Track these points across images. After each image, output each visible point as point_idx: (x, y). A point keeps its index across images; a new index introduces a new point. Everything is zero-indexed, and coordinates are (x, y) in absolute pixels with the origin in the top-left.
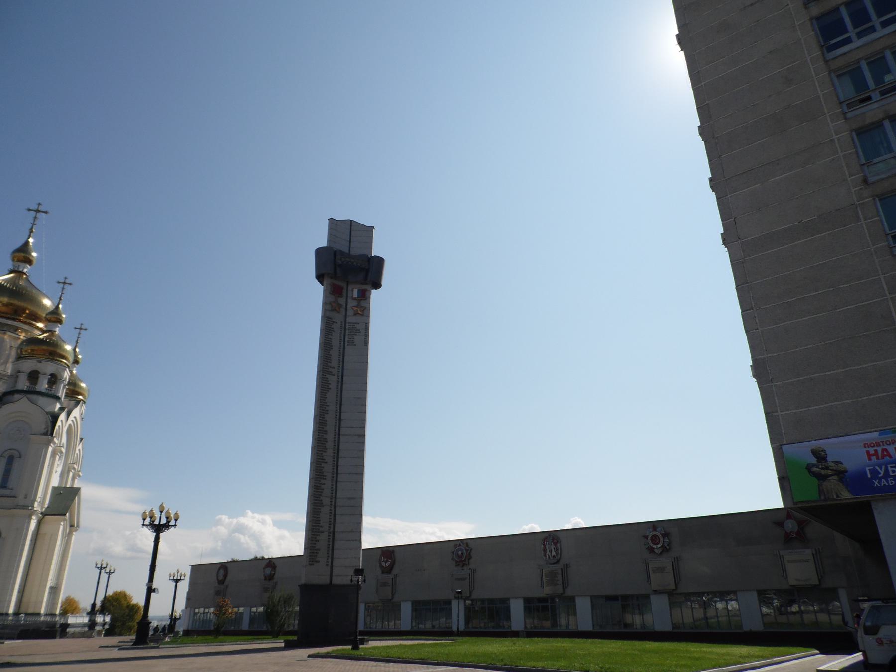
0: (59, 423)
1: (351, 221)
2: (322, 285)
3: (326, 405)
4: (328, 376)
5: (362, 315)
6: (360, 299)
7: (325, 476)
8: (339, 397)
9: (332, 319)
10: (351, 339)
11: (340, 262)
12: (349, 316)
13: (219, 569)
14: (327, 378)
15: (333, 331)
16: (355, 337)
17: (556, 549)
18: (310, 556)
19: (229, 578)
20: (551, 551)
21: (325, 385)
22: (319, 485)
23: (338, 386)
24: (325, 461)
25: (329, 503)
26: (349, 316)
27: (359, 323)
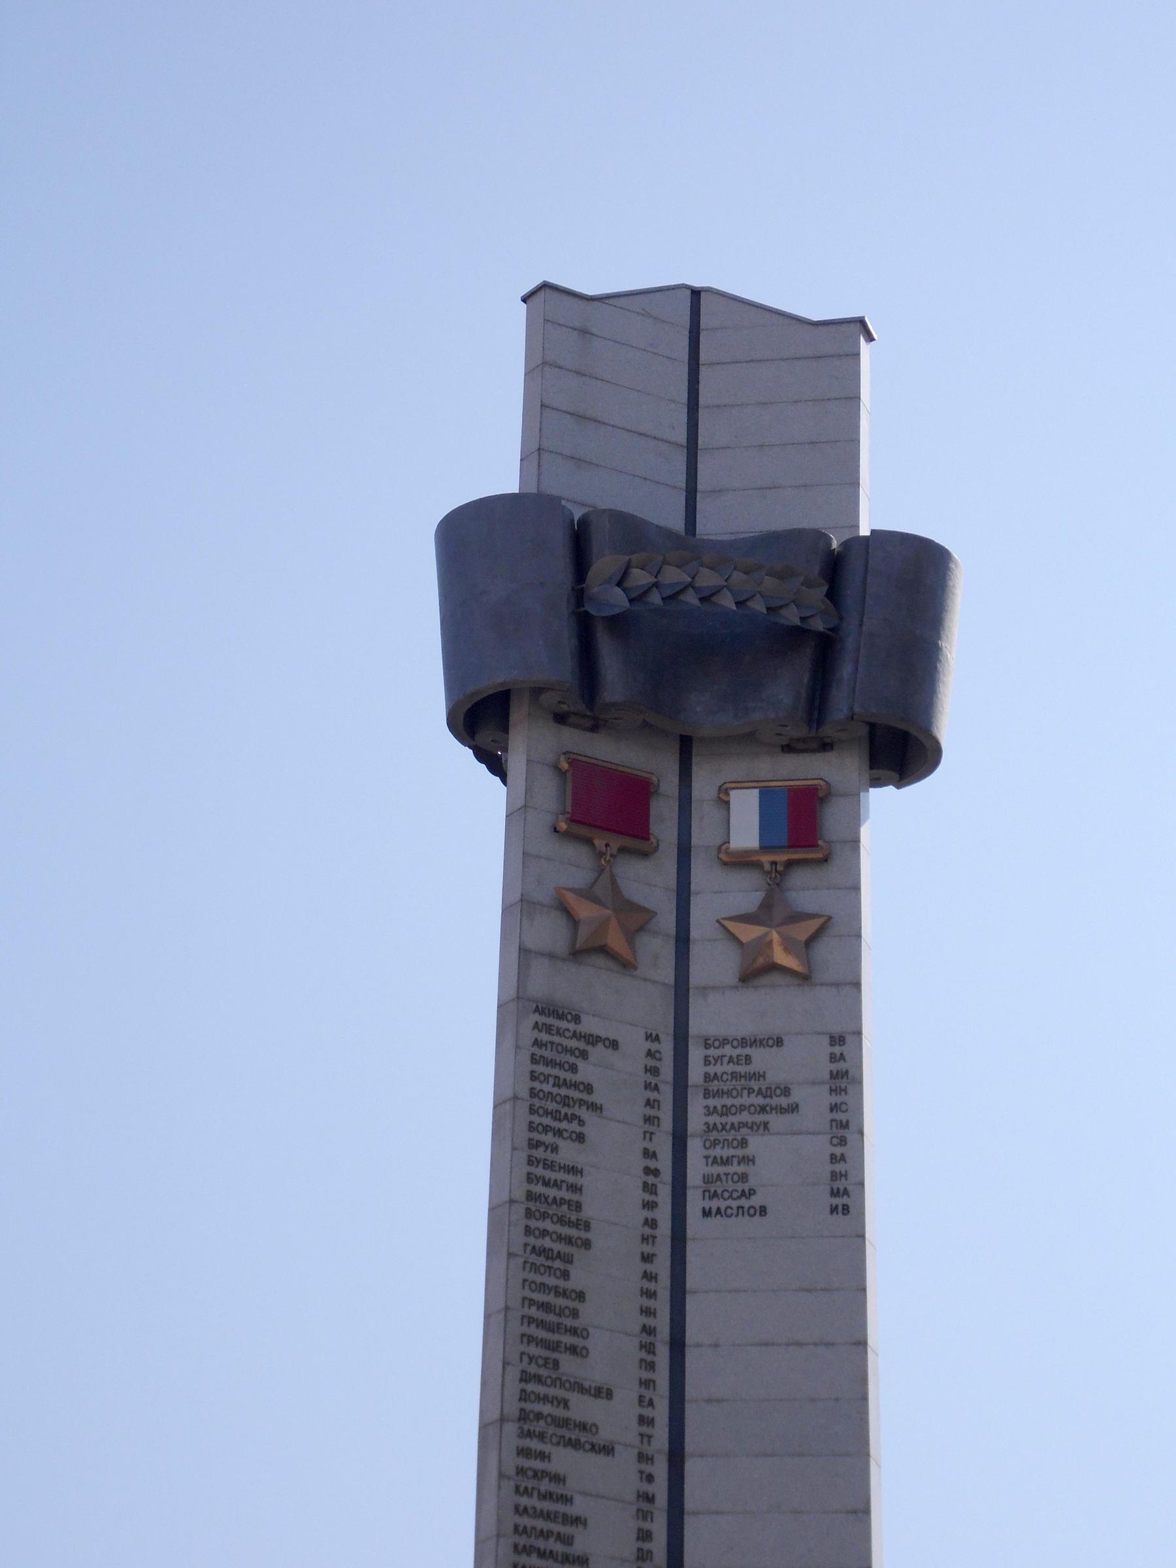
1: (696, 293)
2: (497, 767)
4: (563, 1460)
5: (805, 979)
6: (782, 858)
9: (577, 1019)
10: (726, 1162)
11: (618, 599)
12: (705, 990)
14: (558, 1479)
15: (595, 1108)
16: (757, 1144)
21: (544, 1534)
23: (645, 1536)
26: (705, 990)
27: (779, 1042)
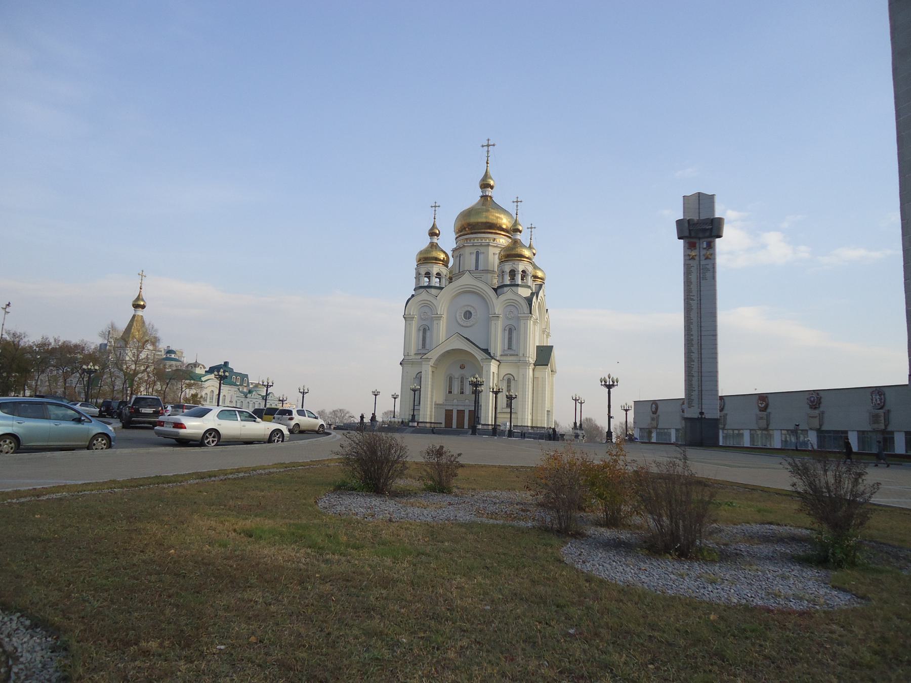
0: (533, 304)
4: (691, 301)
8: (699, 313)
13: (652, 404)
17: (881, 399)
19: (658, 411)
20: (876, 400)
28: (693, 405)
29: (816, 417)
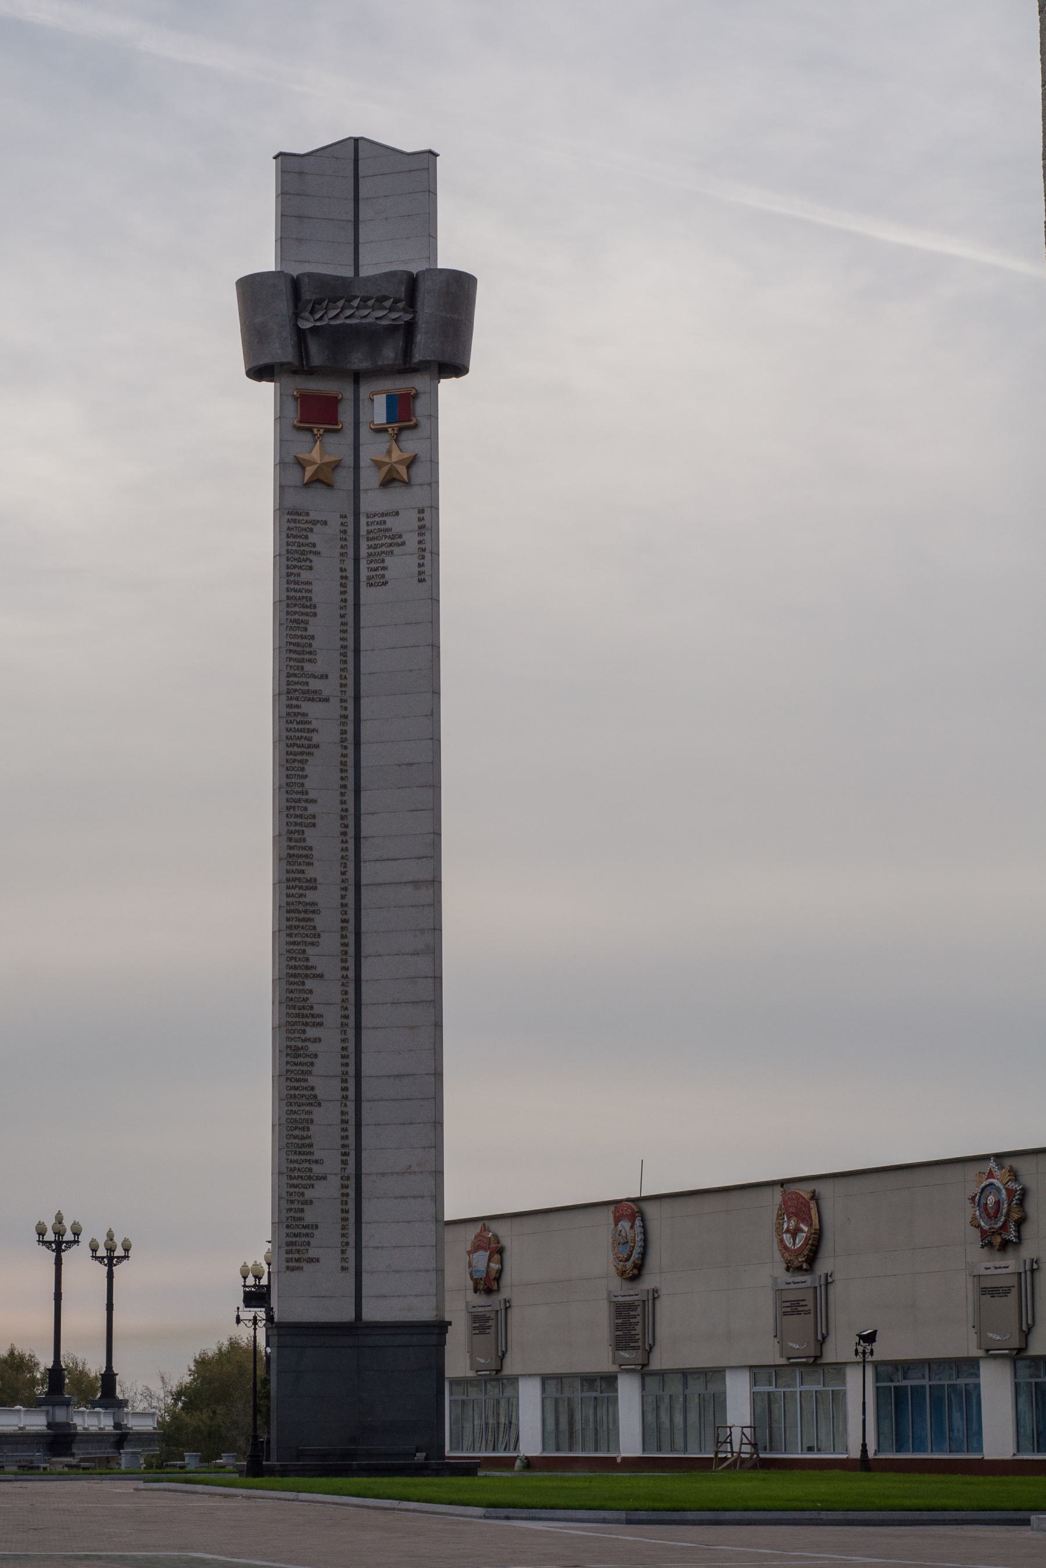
3: (306, 801)
4: (306, 707)
7: (321, 1016)
9: (307, 514)
10: (376, 569)
14: (305, 715)
18: (288, 1244)
22: (300, 1044)
24: (318, 971)
25: (338, 1094)
28: (312, 1253)
29: (1005, 1291)
